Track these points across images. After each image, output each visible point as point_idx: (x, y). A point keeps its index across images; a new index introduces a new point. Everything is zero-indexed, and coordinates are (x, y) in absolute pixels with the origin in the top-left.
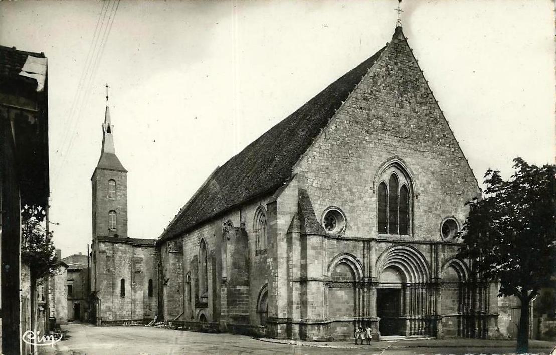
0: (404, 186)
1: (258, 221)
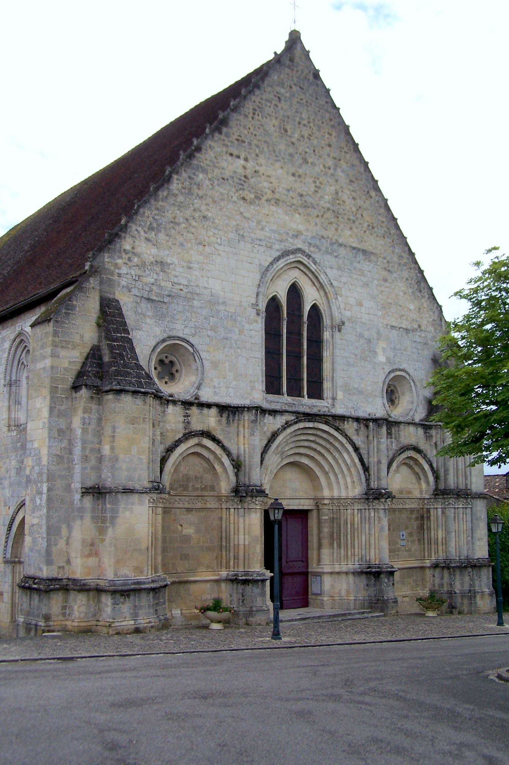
0: (315, 308)
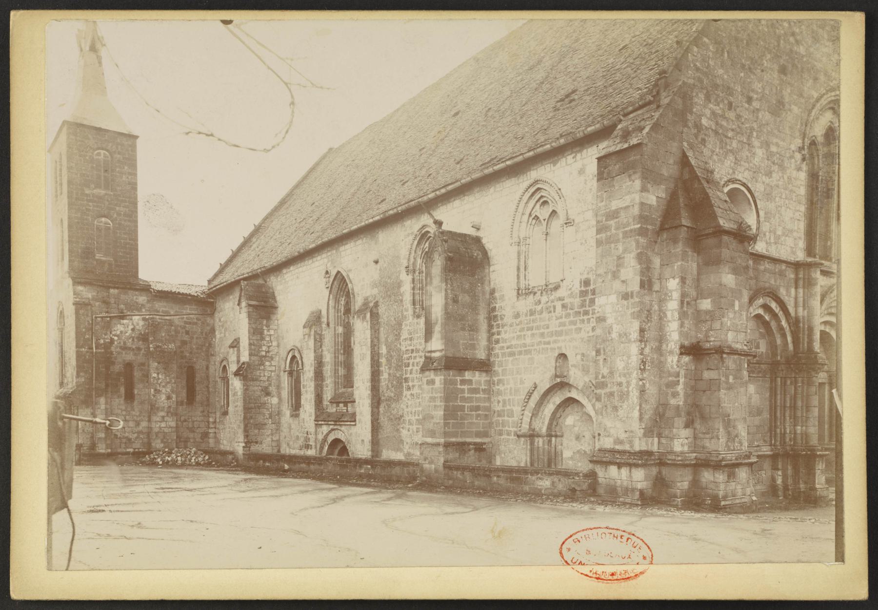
1: (526, 217)
